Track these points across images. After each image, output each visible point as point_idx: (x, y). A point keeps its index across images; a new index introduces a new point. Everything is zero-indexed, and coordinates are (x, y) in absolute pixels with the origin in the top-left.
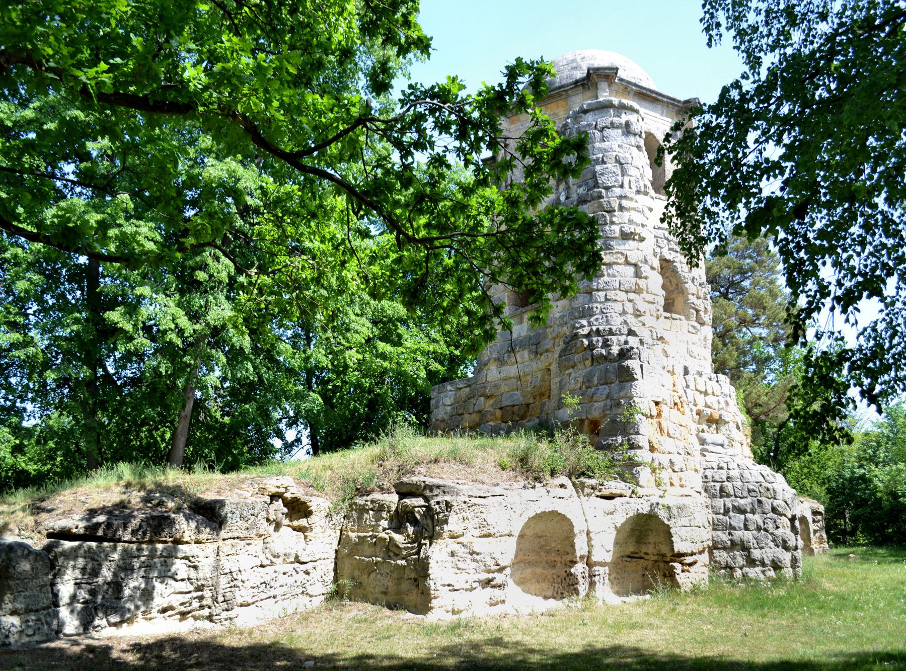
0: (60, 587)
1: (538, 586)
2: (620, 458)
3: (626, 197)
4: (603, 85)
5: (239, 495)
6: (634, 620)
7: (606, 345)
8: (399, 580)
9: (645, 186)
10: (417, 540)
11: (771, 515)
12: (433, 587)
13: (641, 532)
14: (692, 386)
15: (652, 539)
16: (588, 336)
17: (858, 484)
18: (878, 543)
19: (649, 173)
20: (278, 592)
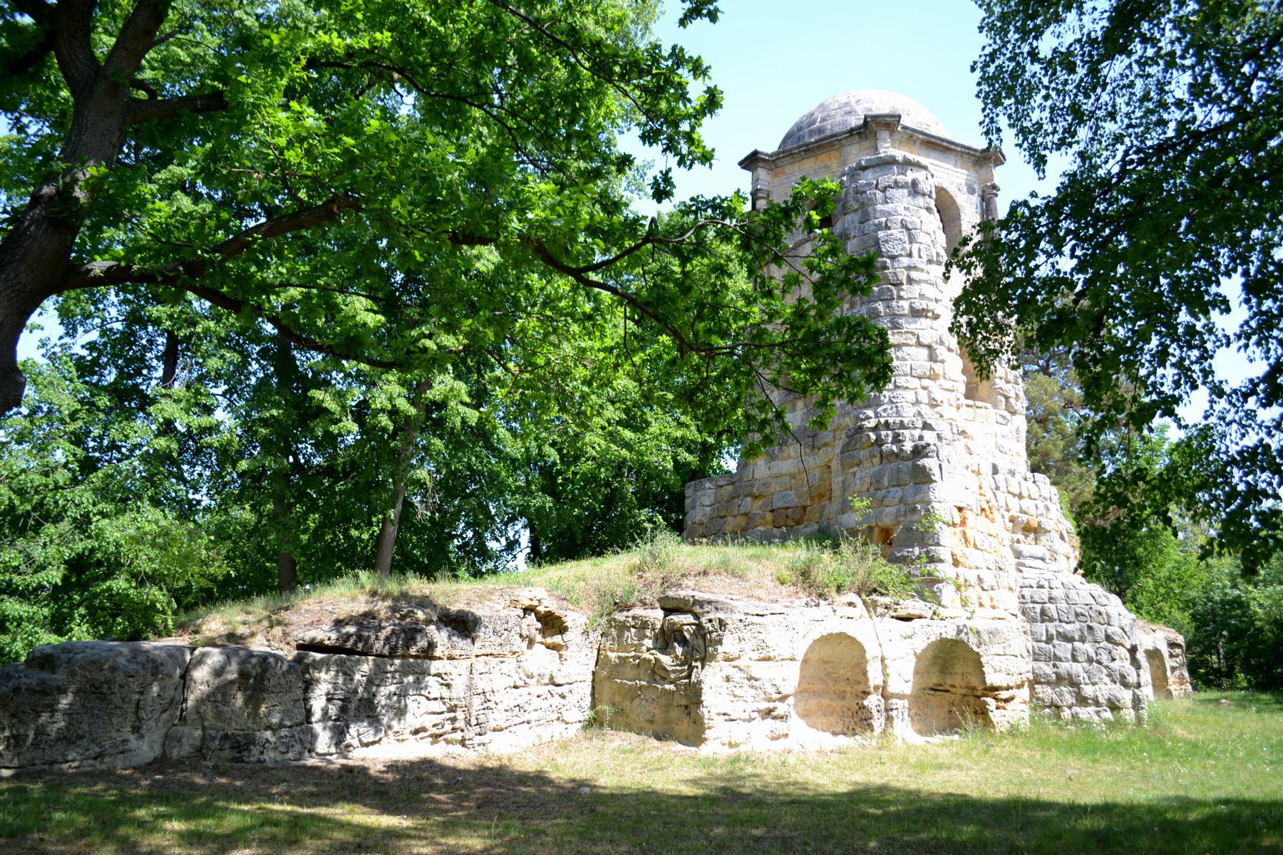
0: (313, 702)
1: (825, 720)
2: (917, 573)
3: (915, 268)
4: (884, 134)
5: (491, 608)
6: (941, 760)
7: (897, 440)
8: (668, 707)
9: (938, 254)
10: (687, 661)
11: (1104, 644)
12: (706, 716)
13: (946, 660)
14: (1003, 488)
15: (959, 669)
16: (875, 429)
17: (1233, 608)
18: (1261, 687)
19: (942, 239)
20: (532, 716)
